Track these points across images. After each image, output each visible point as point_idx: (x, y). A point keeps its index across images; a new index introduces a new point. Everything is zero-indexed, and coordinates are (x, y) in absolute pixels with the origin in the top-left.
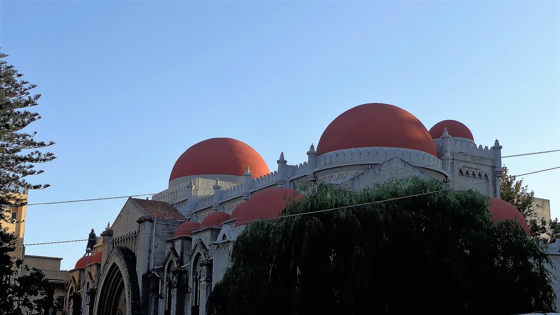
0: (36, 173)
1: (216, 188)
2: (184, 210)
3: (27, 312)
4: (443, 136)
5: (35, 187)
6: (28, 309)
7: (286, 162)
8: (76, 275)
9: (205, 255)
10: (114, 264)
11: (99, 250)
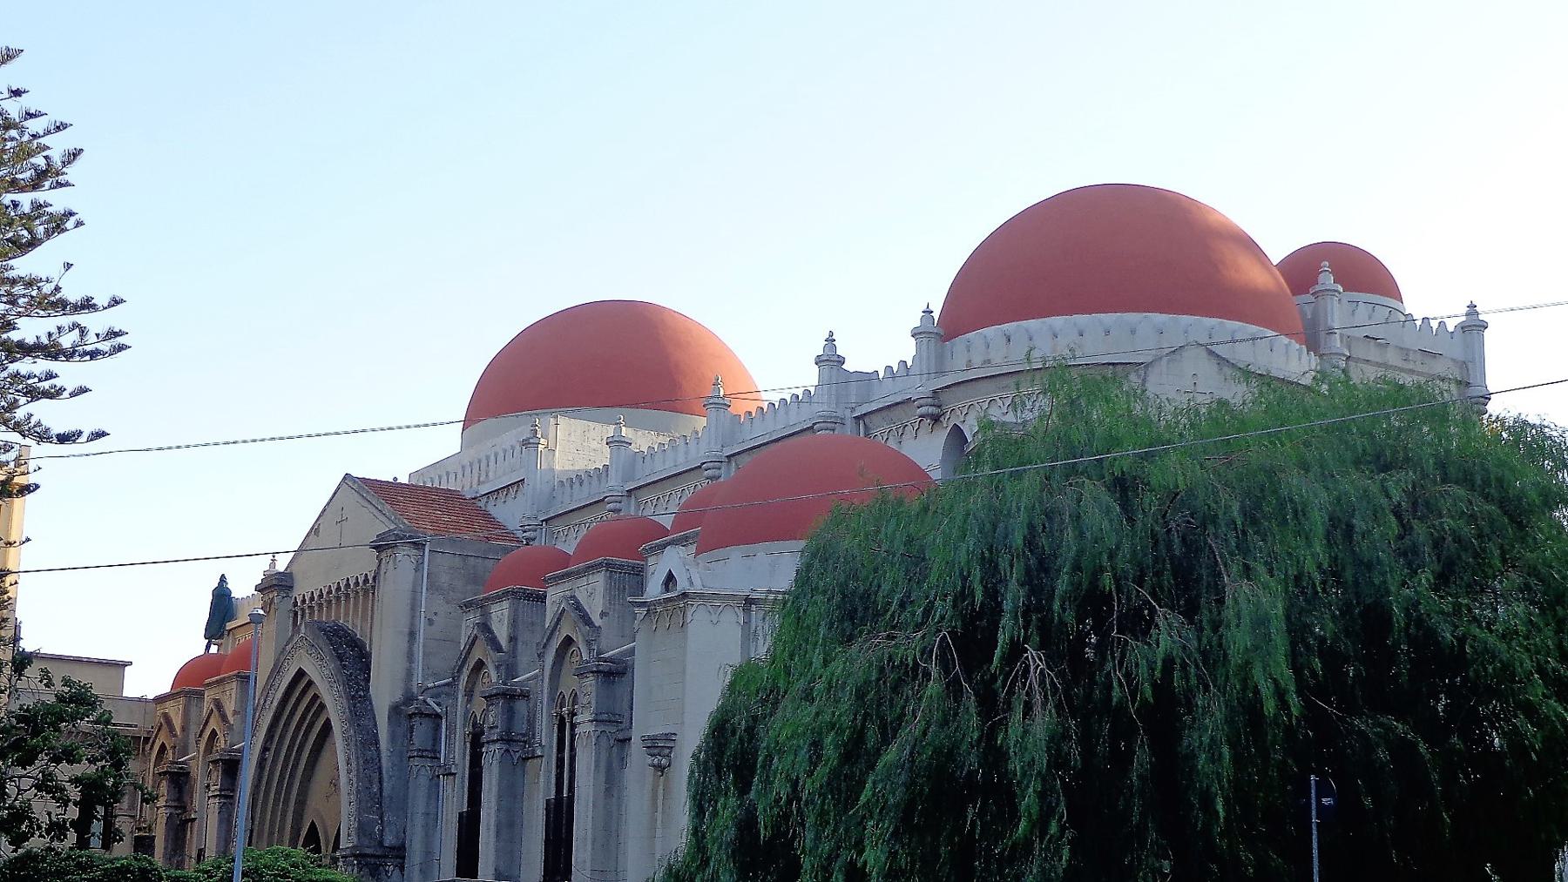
0: (66, 394)
1: (616, 443)
2: (511, 514)
3: (49, 814)
4: (1318, 288)
5: (63, 439)
6: (52, 805)
7: (841, 361)
8: (175, 711)
9: (588, 643)
10: (301, 674)
11: (243, 637)
